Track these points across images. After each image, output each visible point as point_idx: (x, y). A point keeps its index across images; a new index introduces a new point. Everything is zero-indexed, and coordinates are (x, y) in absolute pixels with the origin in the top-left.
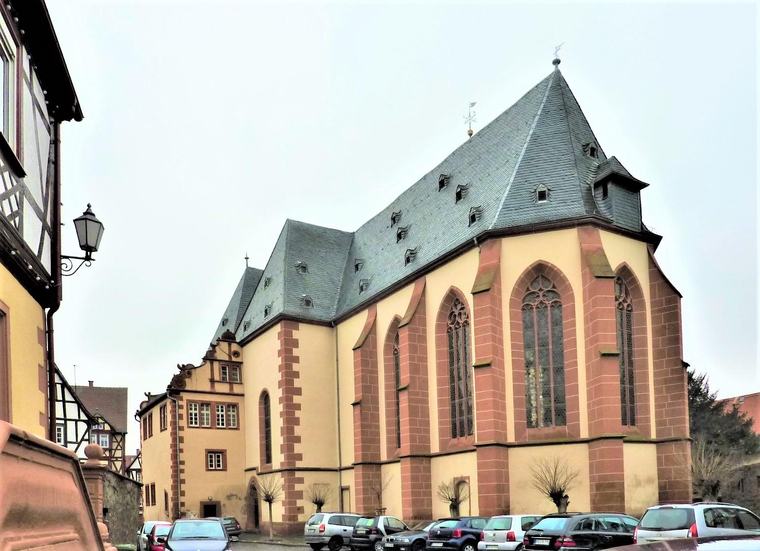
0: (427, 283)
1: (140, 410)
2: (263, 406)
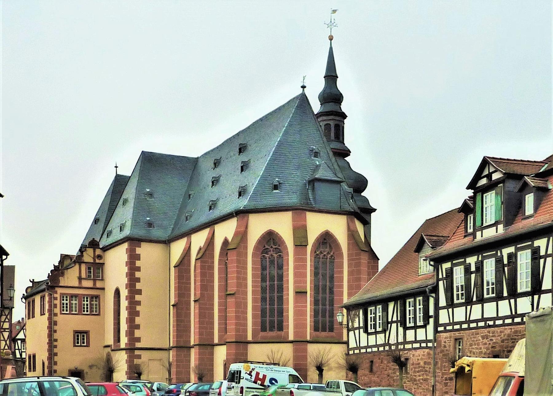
0: (215, 231)
1: (26, 294)
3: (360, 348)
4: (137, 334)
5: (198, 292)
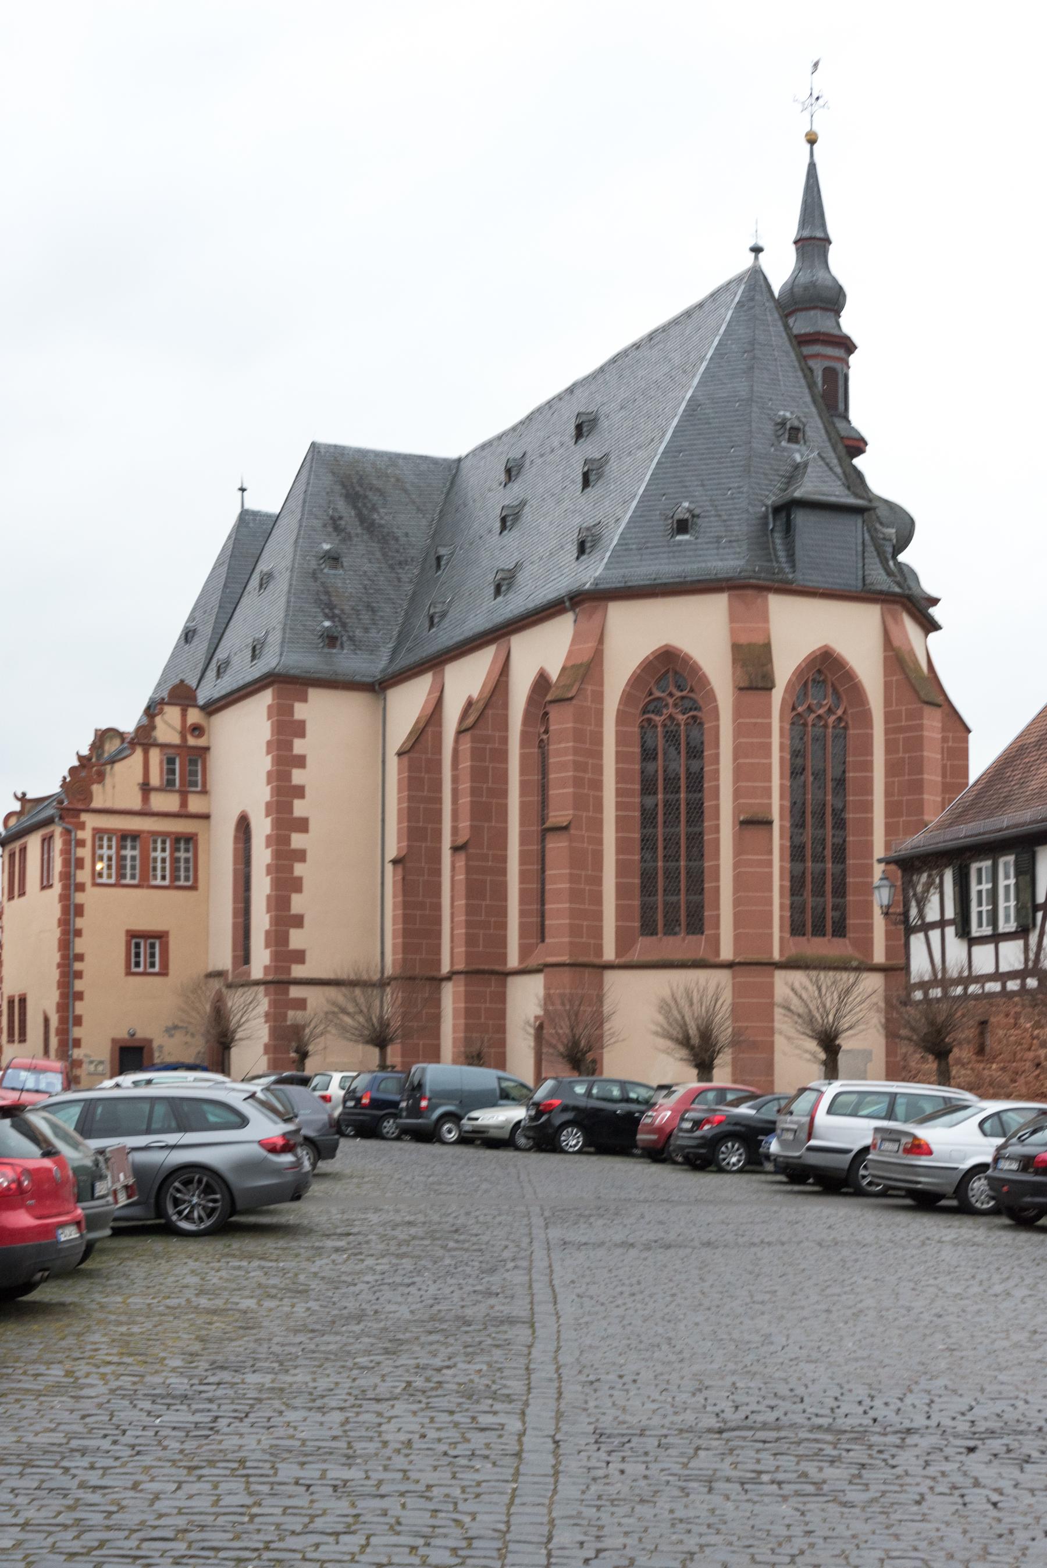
2: (241, 846)
3: (944, 982)
4: (297, 939)
5: (465, 824)
